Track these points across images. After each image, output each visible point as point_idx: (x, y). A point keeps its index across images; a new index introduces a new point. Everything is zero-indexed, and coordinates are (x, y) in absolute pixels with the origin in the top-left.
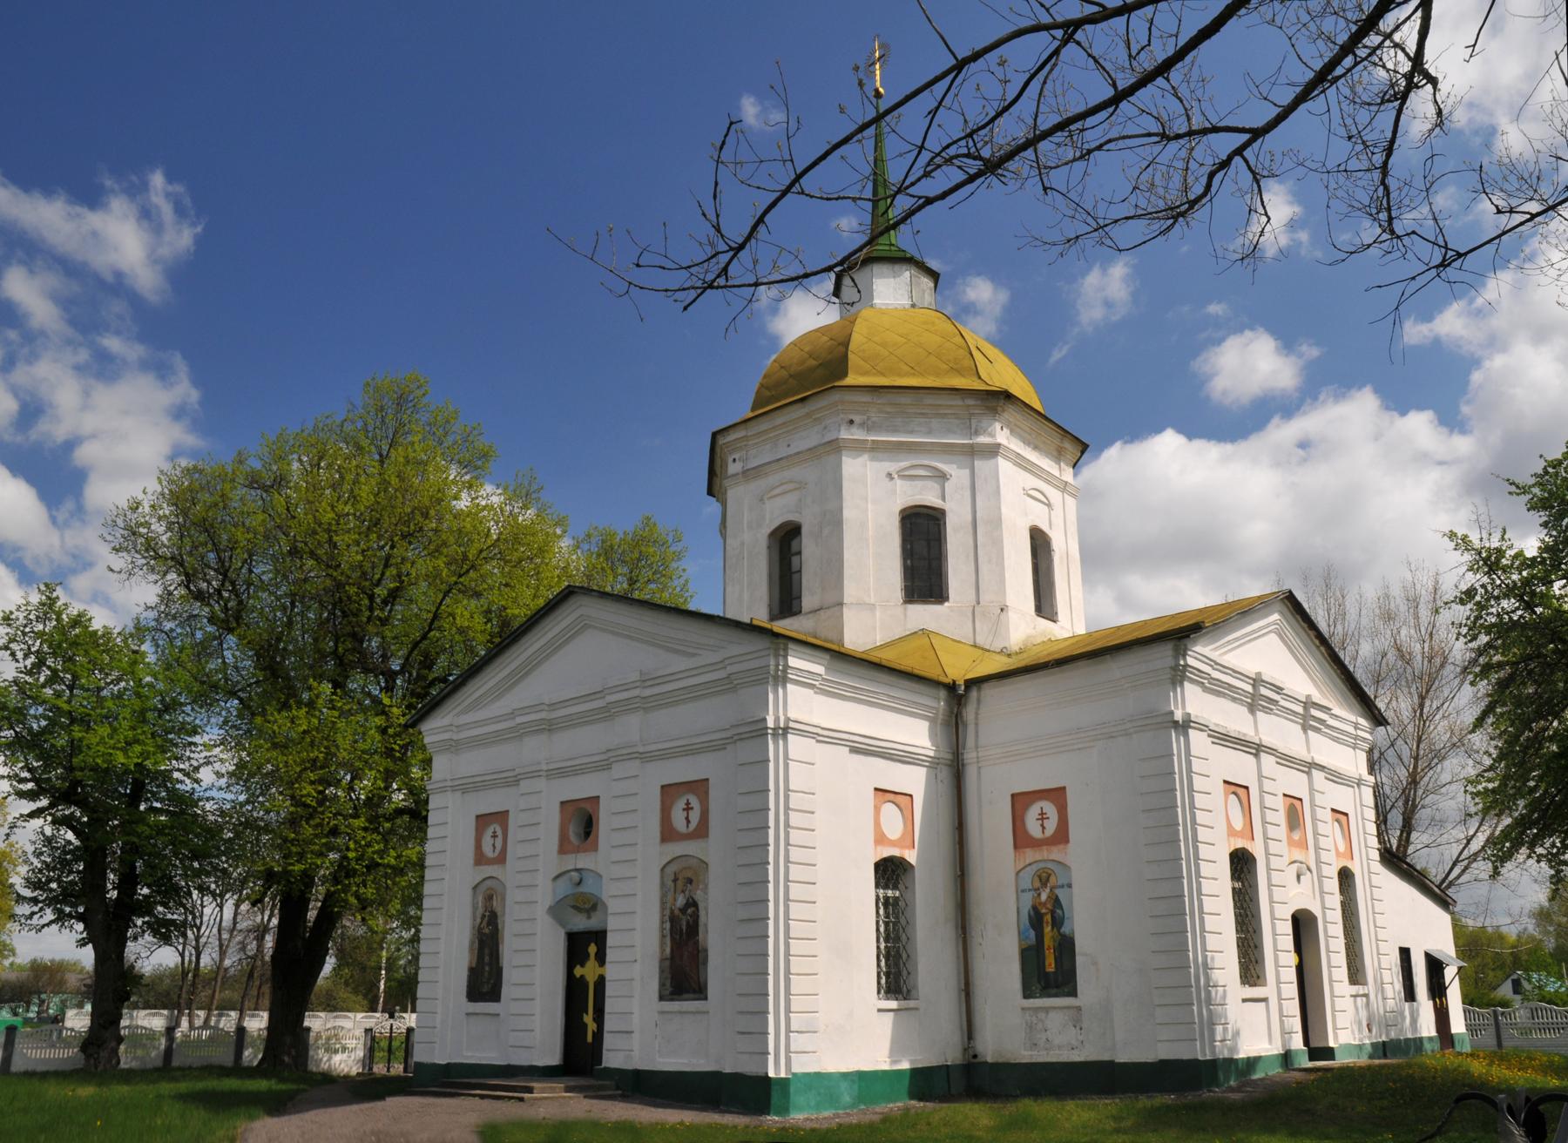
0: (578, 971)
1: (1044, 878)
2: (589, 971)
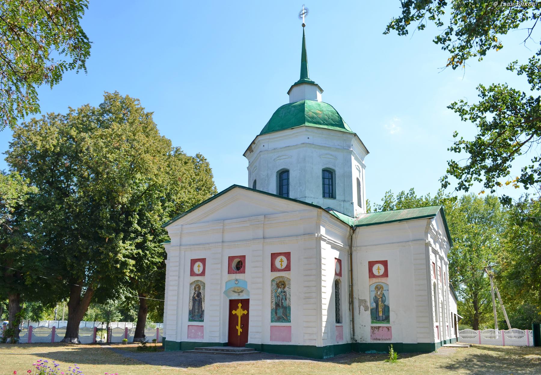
0: (234, 312)
1: (378, 288)
2: (239, 312)
